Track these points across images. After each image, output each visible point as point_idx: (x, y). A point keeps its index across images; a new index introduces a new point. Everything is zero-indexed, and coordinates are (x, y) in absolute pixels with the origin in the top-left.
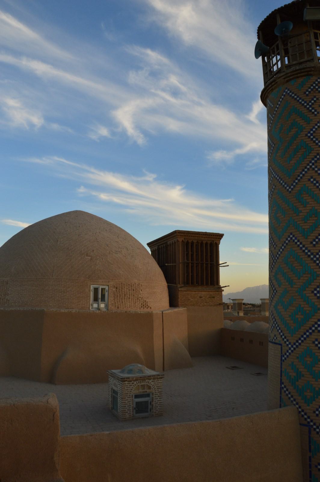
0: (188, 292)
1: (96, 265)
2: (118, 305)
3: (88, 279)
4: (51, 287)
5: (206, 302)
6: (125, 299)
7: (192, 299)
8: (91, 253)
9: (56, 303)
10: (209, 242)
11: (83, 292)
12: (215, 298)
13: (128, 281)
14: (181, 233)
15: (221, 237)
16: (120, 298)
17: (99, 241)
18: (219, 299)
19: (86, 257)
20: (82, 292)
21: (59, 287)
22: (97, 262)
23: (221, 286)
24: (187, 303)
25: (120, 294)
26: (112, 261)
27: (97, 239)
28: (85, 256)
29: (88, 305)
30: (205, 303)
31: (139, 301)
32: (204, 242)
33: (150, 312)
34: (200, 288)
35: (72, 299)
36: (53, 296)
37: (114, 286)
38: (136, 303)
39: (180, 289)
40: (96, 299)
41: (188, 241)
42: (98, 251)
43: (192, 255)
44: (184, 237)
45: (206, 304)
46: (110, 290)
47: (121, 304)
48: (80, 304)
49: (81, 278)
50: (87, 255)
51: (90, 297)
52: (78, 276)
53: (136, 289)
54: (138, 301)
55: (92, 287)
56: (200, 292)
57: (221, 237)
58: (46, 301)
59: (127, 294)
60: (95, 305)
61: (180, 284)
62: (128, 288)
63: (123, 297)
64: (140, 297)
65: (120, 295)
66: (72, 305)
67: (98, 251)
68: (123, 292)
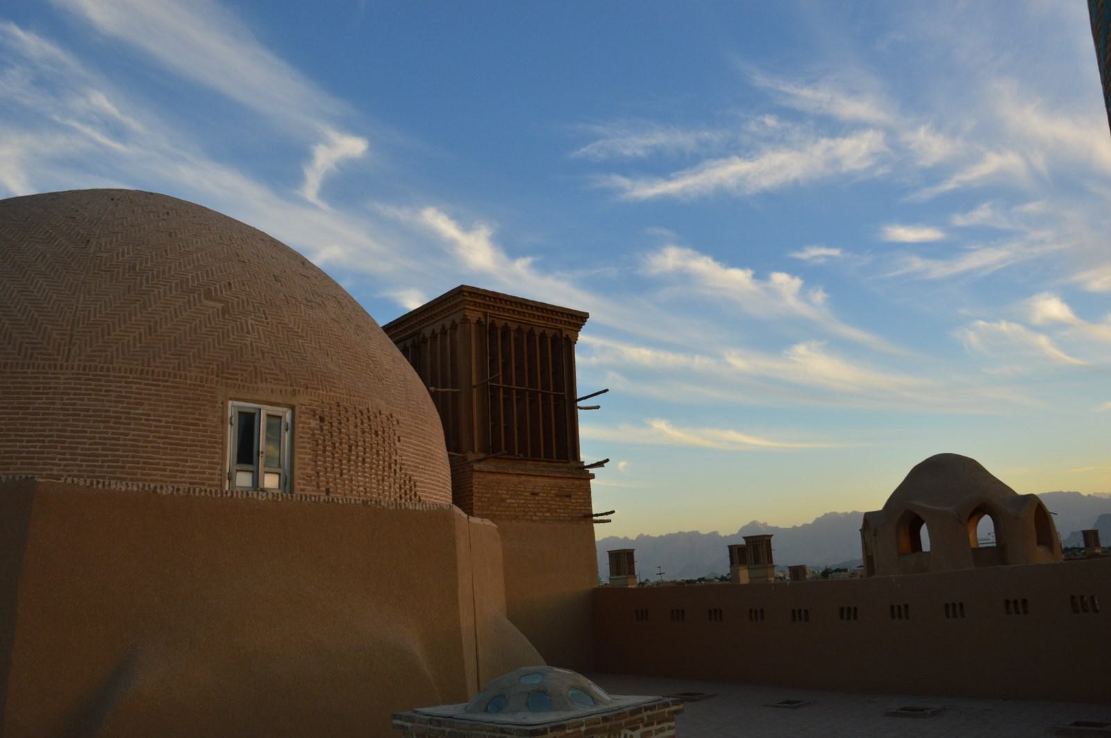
0: (499, 476)
1: (245, 330)
2: (328, 483)
3: (217, 376)
4: (62, 399)
5: (549, 510)
6: (349, 461)
7: (511, 499)
8: (222, 293)
9: (81, 466)
10: (550, 333)
11: (197, 425)
12: (573, 497)
13: (358, 399)
14: (475, 294)
15: (580, 323)
16: (333, 458)
17: (246, 261)
18: (582, 501)
19: (206, 302)
20: (192, 424)
21: (97, 400)
22: (246, 321)
23: (585, 464)
24: (497, 511)
25: (334, 444)
26: (298, 328)
27: (238, 255)
28: (202, 297)
29: (217, 477)
30: (546, 512)
31: (392, 475)
32: (538, 331)
33: (445, 508)
34: (530, 465)
35: (149, 449)
36: (68, 434)
37: (314, 411)
38: (383, 480)
39: (476, 467)
40: (246, 454)
41: (493, 321)
42: (248, 290)
43: (506, 365)
44: (483, 310)
45: (548, 514)
46: (301, 425)
47: (338, 481)
48: (184, 472)
49: (190, 372)
50: (208, 296)
51: (224, 444)
52: (176, 361)
53: (384, 432)
54: (389, 477)
55: (233, 408)
56: (532, 479)
57: (580, 323)
58: (33, 458)
59: (357, 446)
60: (244, 479)
61: (473, 451)
62: (359, 424)
63: (345, 456)
64: (396, 461)
65: (334, 448)
66: (150, 475)
67: (248, 290)
68: (343, 435)
